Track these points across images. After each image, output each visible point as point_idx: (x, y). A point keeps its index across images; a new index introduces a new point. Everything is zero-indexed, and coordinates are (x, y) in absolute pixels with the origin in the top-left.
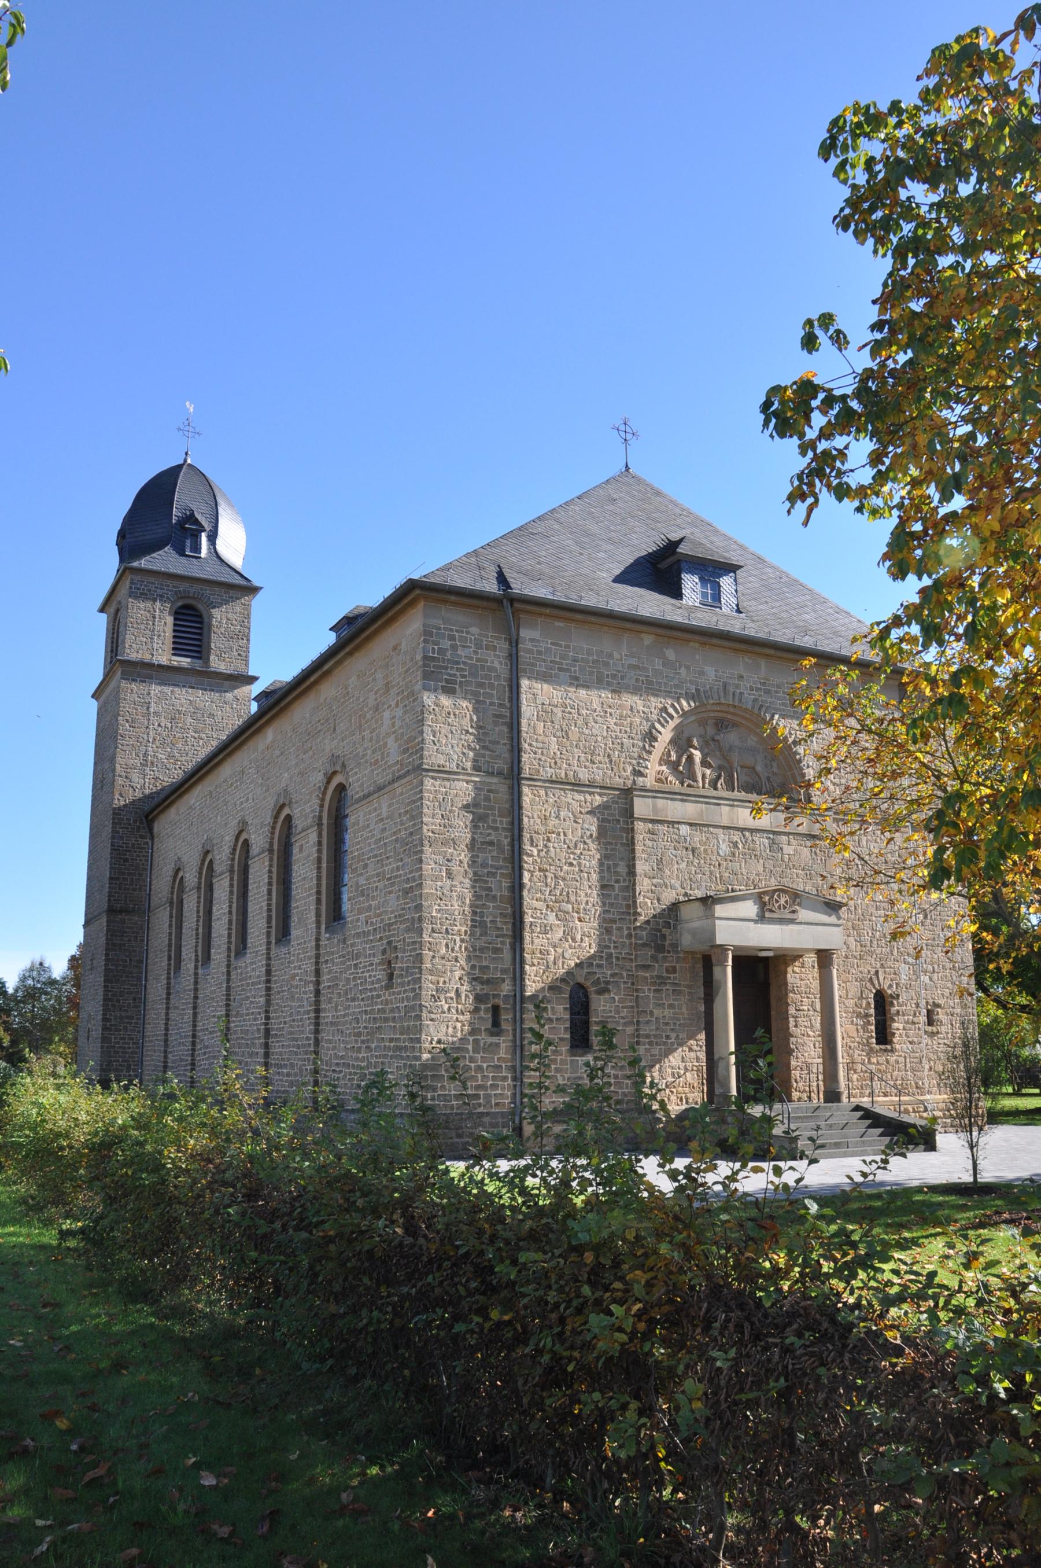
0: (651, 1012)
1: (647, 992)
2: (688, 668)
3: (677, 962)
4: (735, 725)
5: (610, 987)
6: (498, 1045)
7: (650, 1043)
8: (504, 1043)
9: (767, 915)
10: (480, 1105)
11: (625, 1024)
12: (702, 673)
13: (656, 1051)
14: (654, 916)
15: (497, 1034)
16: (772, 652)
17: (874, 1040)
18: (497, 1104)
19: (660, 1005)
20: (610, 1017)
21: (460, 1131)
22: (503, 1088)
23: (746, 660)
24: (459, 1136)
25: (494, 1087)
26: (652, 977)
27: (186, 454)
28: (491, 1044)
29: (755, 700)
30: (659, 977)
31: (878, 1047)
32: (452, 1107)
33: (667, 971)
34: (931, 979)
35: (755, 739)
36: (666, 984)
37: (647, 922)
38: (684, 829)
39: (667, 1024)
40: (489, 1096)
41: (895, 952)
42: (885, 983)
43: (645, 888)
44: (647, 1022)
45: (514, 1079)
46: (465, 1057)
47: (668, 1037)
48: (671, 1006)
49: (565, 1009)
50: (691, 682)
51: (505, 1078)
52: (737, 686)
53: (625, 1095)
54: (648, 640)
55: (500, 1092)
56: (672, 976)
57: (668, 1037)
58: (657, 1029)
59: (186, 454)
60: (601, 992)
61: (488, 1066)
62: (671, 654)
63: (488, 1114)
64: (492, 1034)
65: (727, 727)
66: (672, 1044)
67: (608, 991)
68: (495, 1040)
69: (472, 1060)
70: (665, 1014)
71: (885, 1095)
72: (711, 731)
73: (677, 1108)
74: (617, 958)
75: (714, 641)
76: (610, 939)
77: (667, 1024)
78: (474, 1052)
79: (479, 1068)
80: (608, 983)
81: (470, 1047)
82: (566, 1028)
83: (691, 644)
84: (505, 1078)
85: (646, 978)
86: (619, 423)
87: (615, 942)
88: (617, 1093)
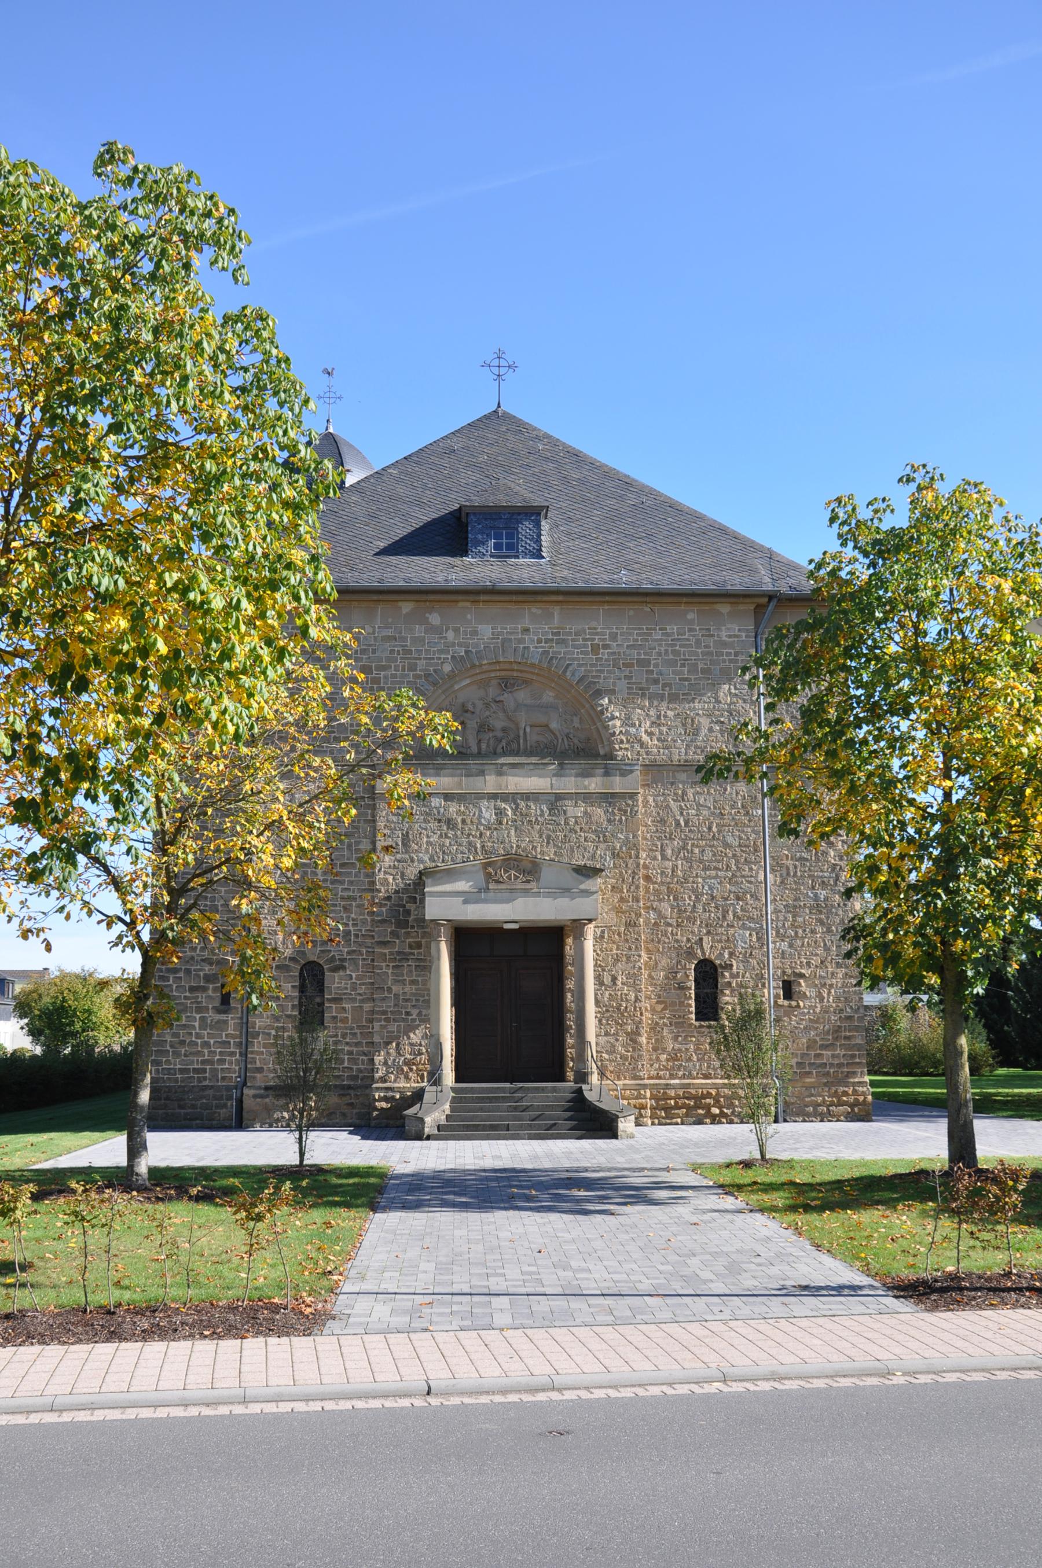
0: (389, 990)
1: (386, 968)
2: (456, 630)
3: (422, 937)
4: (527, 682)
5: (346, 964)
6: (226, 1022)
7: (387, 1020)
8: (232, 1020)
9: (491, 886)
10: (205, 1078)
11: (362, 1001)
12: (475, 633)
13: (393, 1027)
14: (397, 892)
15: (225, 1012)
16: (560, 598)
17: (693, 1016)
18: (223, 1078)
19: (399, 981)
20: (345, 994)
21: (182, 1103)
22: (231, 1063)
23: (534, 610)
24: (181, 1107)
25: (221, 1061)
26: (391, 953)
27: (328, 421)
28: (218, 1022)
29: (545, 653)
30: (399, 953)
31: (697, 1024)
32: (176, 1080)
33: (410, 947)
34: (791, 946)
35: (551, 694)
36: (408, 960)
37: (389, 898)
38: (436, 802)
39: (407, 1000)
40: (216, 1070)
41: (731, 916)
42: (709, 950)
43: (387, 864)
44: (384, 999)
45: (241, 1054)
46: (191, 1034)
47: (408, 1013)
48: (412, 982)
49: (293, 987)
50: (460, 645)
51: (233, 1054)
52: (520, 641)
53: (360, 1071)
54: (407, 607)
55: (227, 1066)
56: (416, 951)
57: (408, 1013)
58: (395, 1005)
59: (328, 421)
60: (335, 969)
61: (215, 1042)
62: (435, 619)
63: (212, 1087)
64: (219, 1011)
65: (513, 685)
66: (414, 1020)
67: (344, 968)
68: (223, 1017)
69: (198, 1036)
70: (406, 990)
71: (706, 1077)
72: (493, 692)
73: (416, 1085)
74: (356, 936)
75: (482, 598)
76: (348, 918)
77: (407, 1000)
78: (200, 1029)
79: (206, 1044)
80: (343, 960)
81: (197, 1024)
82: (293, 1006)
83: (461, 604)
84: (233, 1054)
85: (385, 954)
86: (489, 357)
87: (353, 920)
88: (351, 1069)
